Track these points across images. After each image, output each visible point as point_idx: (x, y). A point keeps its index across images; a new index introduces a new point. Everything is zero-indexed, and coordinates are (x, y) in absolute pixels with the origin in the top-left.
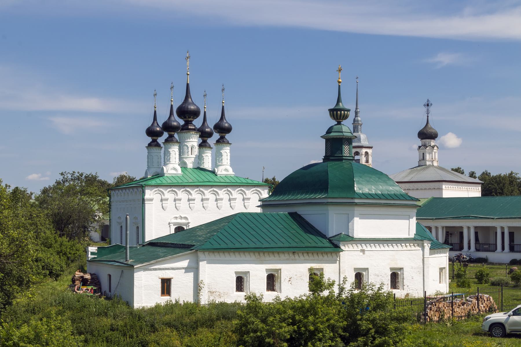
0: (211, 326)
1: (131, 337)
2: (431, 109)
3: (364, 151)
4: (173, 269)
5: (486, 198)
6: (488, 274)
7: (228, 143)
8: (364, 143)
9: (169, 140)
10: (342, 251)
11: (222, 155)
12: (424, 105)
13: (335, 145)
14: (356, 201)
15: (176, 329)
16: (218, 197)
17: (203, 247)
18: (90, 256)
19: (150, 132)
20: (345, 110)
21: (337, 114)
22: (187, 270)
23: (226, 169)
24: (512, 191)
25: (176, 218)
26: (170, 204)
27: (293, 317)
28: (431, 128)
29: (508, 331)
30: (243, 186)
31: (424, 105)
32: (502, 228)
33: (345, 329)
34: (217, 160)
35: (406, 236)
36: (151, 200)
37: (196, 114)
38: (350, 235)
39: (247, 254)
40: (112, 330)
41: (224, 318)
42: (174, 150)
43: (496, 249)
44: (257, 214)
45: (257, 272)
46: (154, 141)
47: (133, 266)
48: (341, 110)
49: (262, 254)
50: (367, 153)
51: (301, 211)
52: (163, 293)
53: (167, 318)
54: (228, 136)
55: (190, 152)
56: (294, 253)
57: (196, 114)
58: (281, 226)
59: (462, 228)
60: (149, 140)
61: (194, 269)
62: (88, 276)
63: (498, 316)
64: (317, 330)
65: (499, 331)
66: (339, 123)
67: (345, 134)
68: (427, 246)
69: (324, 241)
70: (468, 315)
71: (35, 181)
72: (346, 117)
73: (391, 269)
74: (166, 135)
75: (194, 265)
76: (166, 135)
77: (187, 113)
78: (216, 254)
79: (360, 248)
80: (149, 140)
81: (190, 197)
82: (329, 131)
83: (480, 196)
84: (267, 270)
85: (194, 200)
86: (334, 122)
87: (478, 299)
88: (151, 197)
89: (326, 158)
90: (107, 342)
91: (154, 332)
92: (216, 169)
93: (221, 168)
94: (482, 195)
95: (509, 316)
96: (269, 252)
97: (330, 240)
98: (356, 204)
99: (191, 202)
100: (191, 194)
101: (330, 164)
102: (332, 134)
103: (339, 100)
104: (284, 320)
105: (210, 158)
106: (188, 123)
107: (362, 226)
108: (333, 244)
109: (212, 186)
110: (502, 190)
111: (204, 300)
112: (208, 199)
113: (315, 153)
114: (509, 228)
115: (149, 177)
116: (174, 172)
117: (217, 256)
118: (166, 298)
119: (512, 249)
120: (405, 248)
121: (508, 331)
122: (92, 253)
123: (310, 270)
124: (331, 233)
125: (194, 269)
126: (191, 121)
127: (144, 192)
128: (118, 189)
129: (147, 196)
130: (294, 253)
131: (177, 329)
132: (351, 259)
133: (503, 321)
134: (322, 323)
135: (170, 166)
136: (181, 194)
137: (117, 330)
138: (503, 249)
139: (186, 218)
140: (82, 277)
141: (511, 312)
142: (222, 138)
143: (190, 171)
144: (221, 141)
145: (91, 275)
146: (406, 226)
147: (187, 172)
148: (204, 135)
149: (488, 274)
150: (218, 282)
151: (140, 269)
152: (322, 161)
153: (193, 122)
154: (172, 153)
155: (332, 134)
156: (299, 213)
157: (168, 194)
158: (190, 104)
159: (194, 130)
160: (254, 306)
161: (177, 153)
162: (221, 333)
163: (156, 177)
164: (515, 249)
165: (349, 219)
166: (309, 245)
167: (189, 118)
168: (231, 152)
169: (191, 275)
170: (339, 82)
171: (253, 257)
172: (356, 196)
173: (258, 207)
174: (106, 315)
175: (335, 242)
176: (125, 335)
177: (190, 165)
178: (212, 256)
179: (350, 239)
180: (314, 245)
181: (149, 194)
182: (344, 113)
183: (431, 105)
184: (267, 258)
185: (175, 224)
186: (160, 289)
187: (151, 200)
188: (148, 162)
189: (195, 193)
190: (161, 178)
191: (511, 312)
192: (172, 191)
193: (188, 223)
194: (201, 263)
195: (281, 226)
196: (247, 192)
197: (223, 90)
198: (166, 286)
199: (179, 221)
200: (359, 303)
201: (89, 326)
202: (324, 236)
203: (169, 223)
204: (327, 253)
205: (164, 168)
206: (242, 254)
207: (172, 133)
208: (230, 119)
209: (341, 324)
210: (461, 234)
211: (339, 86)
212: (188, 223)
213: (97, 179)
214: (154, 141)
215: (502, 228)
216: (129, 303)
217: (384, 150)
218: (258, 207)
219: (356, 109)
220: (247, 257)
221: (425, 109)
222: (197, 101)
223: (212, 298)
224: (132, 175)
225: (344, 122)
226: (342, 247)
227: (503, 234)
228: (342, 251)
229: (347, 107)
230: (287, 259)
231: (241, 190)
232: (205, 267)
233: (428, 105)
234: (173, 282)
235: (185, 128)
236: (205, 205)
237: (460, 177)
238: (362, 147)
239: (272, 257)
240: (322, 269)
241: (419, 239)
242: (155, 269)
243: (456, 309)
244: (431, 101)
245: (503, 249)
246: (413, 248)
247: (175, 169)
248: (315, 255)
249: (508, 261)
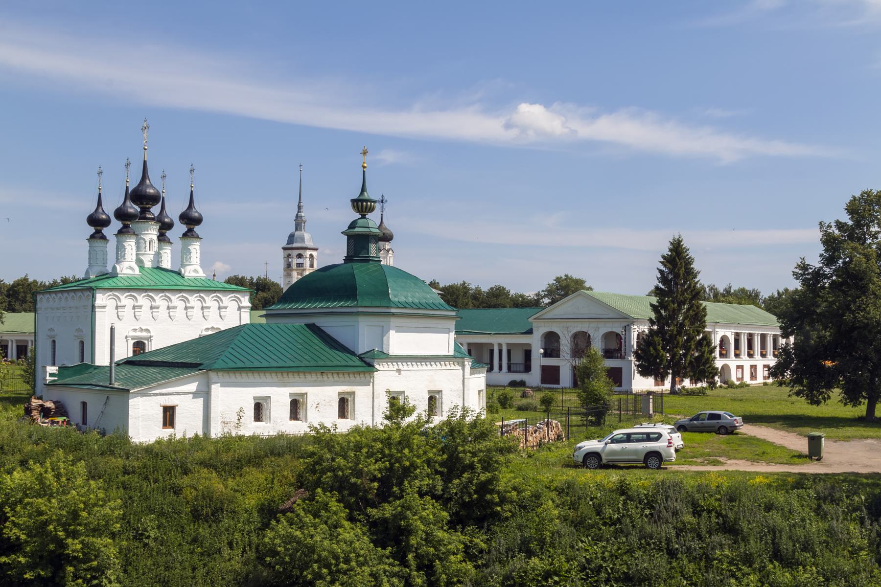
0: (258, 465)
1: (156, 481)
3: (308, 253)
4: (178, 394)
6: (512, 398)
7: (198, 237)
8: (308, 243)
9: (123, 232)
10: (377, 370)
11: (190, 253)
13: (360, 243)
14: (393, 310)
15: (215, 469)
16: (188, 305)
17: (216, 366)
20: (371, 201)
21: (362, 205)
22: (196, 395)
23: (194, 270)
24: (467, 304)
25: (135, 330)
26: (127, 313)
27: (382, 451)
28: (386, 229)
29: (604, 461)
30: (219, 291)
32: (500, 345)
33: (442, 464)
34: (184, 256)
35: (446, 353)
36: (104, 307)
37: (155, 199)
38: (385, 351)
39: (268, 375)
40: (126, 472)
41: (272, 453)
42: (130, 244)
44: (261, 325)
45: (279, 396)
46: (98, 232)
47: (128, 391)
48: (367, 201)
49: (285, 375)
50: (311, 256)
51: (320, 322)
52: (165, 425)
53: (198, 455)
54: (197, 229)
55: (148, 248)
56: (322, 373)
58: (300, 341)
59: (492, 345)
60: (92, 230)
61: (205, 394)
62: (49, 405)
63: (592, 445)
64: (413, 466)
65: (593, 461)
66: (363, 217)
67: (372, 230)
68: (468, 364)
69: (354, 358)
70: (540, 445)
71: (9, 281)
72: (371, 210)
73: (429, 392)
75: (204, 389)
78: (232, 375)
79: (396, 367)
80: (92, 230)
81: (154, 304)
82: (353, 225)
84: (340, 393)
85: (158, 308)
87: (547, 426)
88: (103, 303)
89: (348, 259)
90: (124, 489)
91: (186, 474)
92: (183, 270)
93: (188, 268)
95: (606, 444)
96: (293, 372)
97: (361, 358)
98: (393, 315)
100: (154, 300)
101: (356, 265)
102: (357, 230)
103: (363, 189)
104: (370, 455)
105: (170, 255)
106: (145, 210)
107: (400, 341)
108: (365, 362)
109: (181, 291)
110: (456, 302)
111: (216, 432)
112: (175, 307)
114: (508, 344)
115: (92, 277)
116: (130, 272)
117: (232, 378)
118: (169, 431)
119: (509, 369)
120: (444, 367)
121: (604, 461)
122: (51, 375)
123: (340, 393)
124: (361, 349)
125: (205, 394)
126: (149, 208)
127: (94, 297)
128: (50, 293)
129: (98, 302)
130: (322, 373)
131: (217, 472)
132: (386, 378)
133: (599, 451)
134: (419, 457)
135: (125, 264)
136: (142, 300)
137: (134, 472)
138: (500, 368)
139: (147, 331)
140: (41, 406)
141: (608, 440)
142: (190, 230)
143: (149, 271)
144: (189, 235)
145: (54, 403)
146: (442, 342)
147: (144, 272)
148: (165, 227)
149: (512, 398)
150: (230, 409)
151: (137, 394)
153: (151, 210)
154: (128, 249)
155: (357, 230)
156: (317, 324)
157: (125, 300)
158: (148, 186)
159: (153, 219)
160: (322, 439)
161: (134, 248)
162: (273, 473)
163: (106, 278)
164: (512, 369)
165: (384, 332)
166: (339, 364)
167: (147, 204)
168: (200, 249)
169: (200, 401)
170: (364, 167)
171: (274, 378)
172: (393, 305)
174: (112, 453)
175: (368, 360)
176: (146, 478)
177: (148, 264)
178: (226, 377)
179: (386, 357)
180: (344, 363)
181: (101, 299)
184: (291, 379)
185: (133, 338)
186: (162, 420)
187: (104, 307)
188: (89, 259)
189: (159, 300)
190: (114, 280)
191: (608, 440)
192: (131, 295)
193: (151, 337)
194: (213, 386)
195: (300, 341)
196: (223, 299)
197: (192, 171)
198: (169, 415)
199: (139, 334)
200: (459, 432)
201: (95, 469)
202: (353, 353)
203: (126, 337)
204: (359, 373)
205: (118, 267)
206: (262, 375)
207: (128, 223)
208: (200, 208)
209: (440, 458)
210: (492, 351)
212: (151, 337)
213: (815, 262)
214: (98, 232)
215: (500, 345)
216: (124, 437)
217: (419, 253)
219: (300, 202)
220: (268, 377)
223: (226, 430)
224: (69, 275)
225: (369, 216)
226: (377, 366)
227: (500, 351)
228: (377, 370)
229: (373, 198)
230: (315, 381)
231: (217, 296)
232: (218, 392)
234: (177, 410)
235: (143, 216)
236: (171, 314)
238: (306, 248)
239: (297, 378)
240: (354, 393)
241: (456, 358)
242: (156, 395)
243: (529, 438)
245: (500, 368)
246: (453, 367)
247: (131, 268)
248: (346, 376)
249: (506, 382)
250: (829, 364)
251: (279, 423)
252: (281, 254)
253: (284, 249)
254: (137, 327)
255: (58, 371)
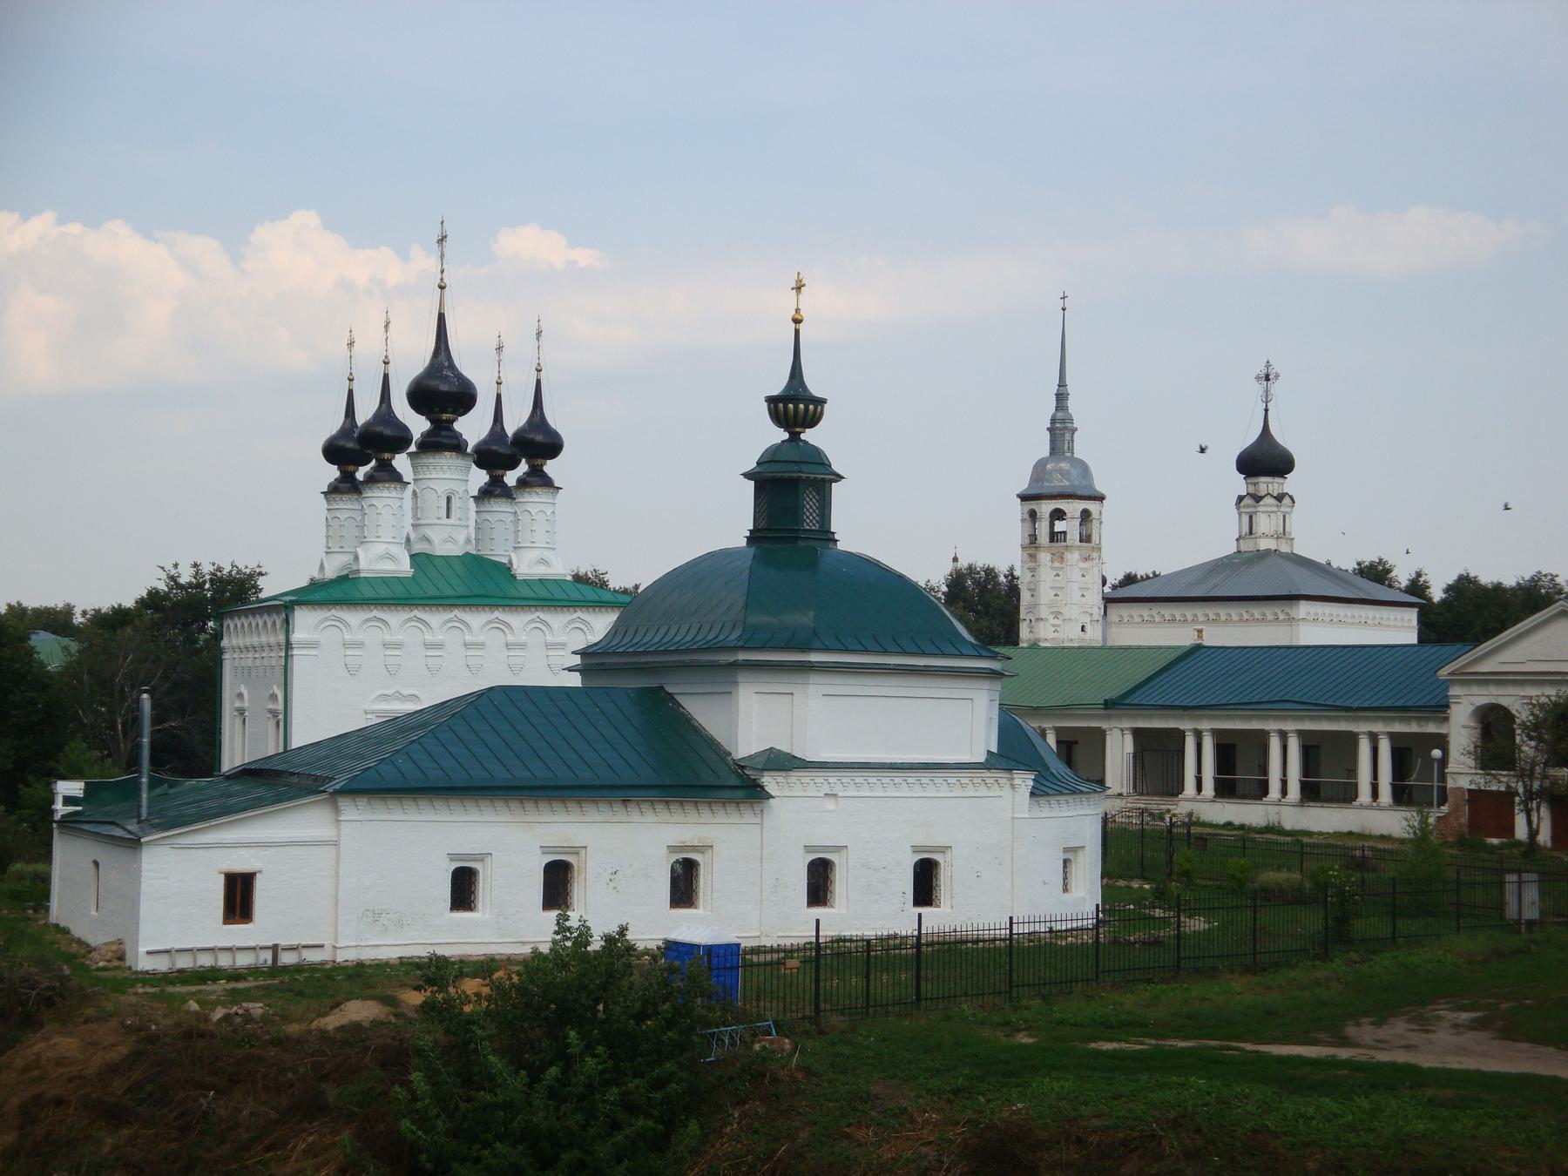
2: (1276, 387)
5: (1430, 650)
12: (1258, 378)
18: (60, 809)
19: (332, 452)
31: (1258, 378)
36: (314, 645)
43: (1265, 792)
50: (1086, 515)
54: (551, 467)
57: (464, 399)
60: (333, 472)
74: (523, 467)
76: (523, 467)
77: (443, 393)
83: (1415, 641)
86: (782, 435)
88: (314, 636)
94: (1422, 639)
99: (349, 652)
113: (730, 520)
119: (1402, 796)
122: (68, 800)
129: (297, 636)
132: (797, 817)
152: (743, 543)
160: (868, 957)
173: (570, 669)
182: (796, 408)
183: (1277, 376)
211: (797, 332)
218: (570, 669)
219: (1062, 384)
221: (1259, 388)
222: (470, 363)
233: (1267, 378)
234: (260, 886)
237: (1359, 589)
244: (1277, 367)
250: (1495, 841)
251: (510, 924)
252: (1017, 509)
253: (1024, 498)
254: (390, 692)
255: (86, 791)
